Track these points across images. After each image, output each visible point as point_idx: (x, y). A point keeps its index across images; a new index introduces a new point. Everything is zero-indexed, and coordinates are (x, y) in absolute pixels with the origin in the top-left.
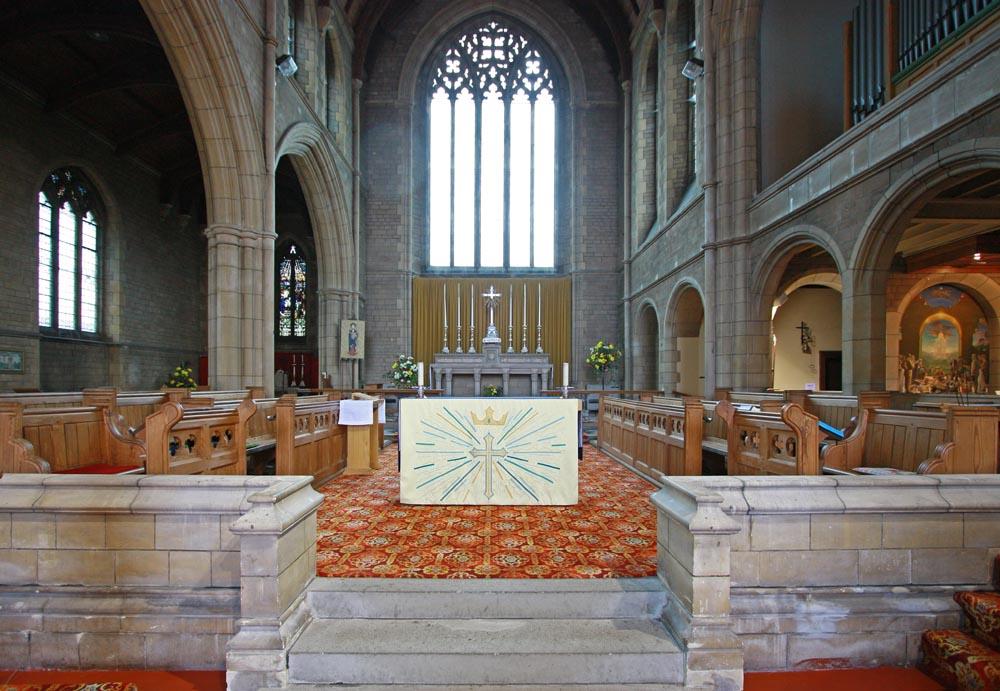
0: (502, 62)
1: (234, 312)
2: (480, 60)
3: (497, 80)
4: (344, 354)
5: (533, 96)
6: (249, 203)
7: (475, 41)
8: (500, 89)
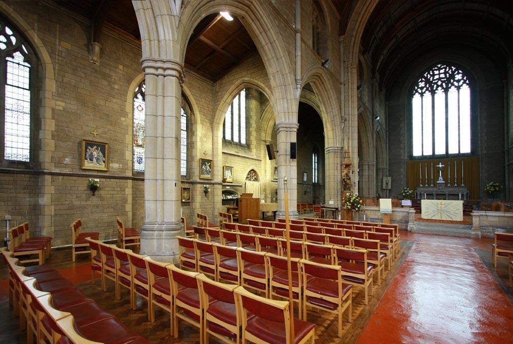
0: (444, 78)
1: (367, 180)
2: (433, 80)
3: (441, 86)
4: (384, 187)
5: (458, 88)
6: (370, 155)
7: (431, 73)
8: (443, 88)
